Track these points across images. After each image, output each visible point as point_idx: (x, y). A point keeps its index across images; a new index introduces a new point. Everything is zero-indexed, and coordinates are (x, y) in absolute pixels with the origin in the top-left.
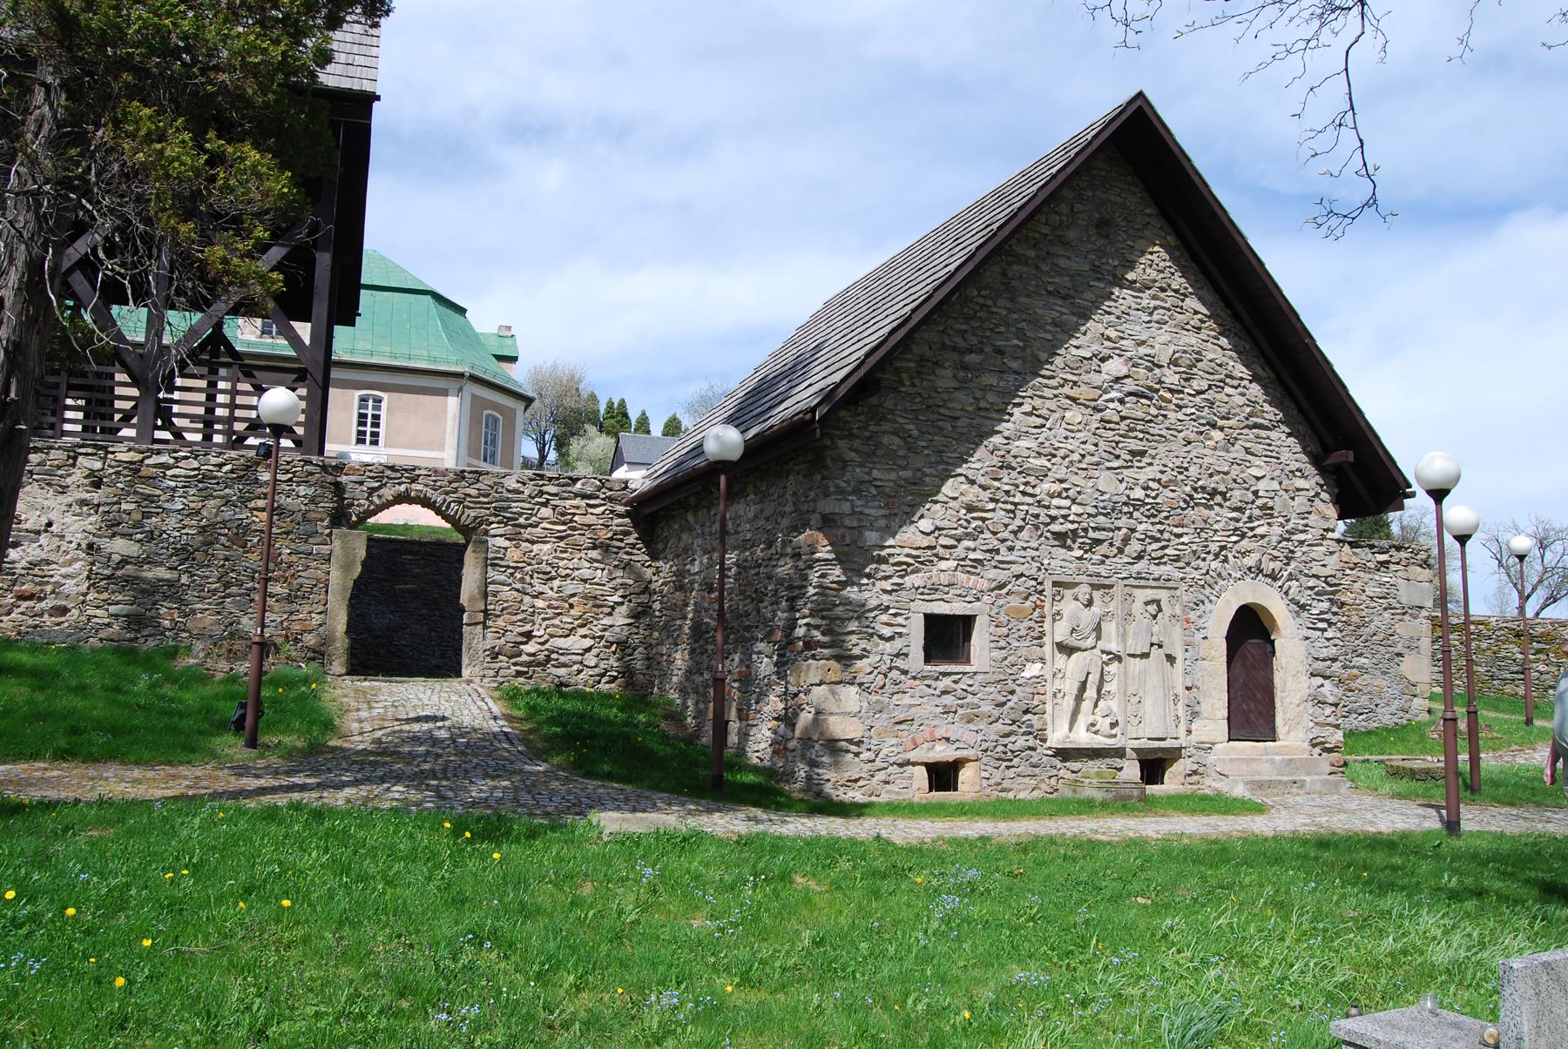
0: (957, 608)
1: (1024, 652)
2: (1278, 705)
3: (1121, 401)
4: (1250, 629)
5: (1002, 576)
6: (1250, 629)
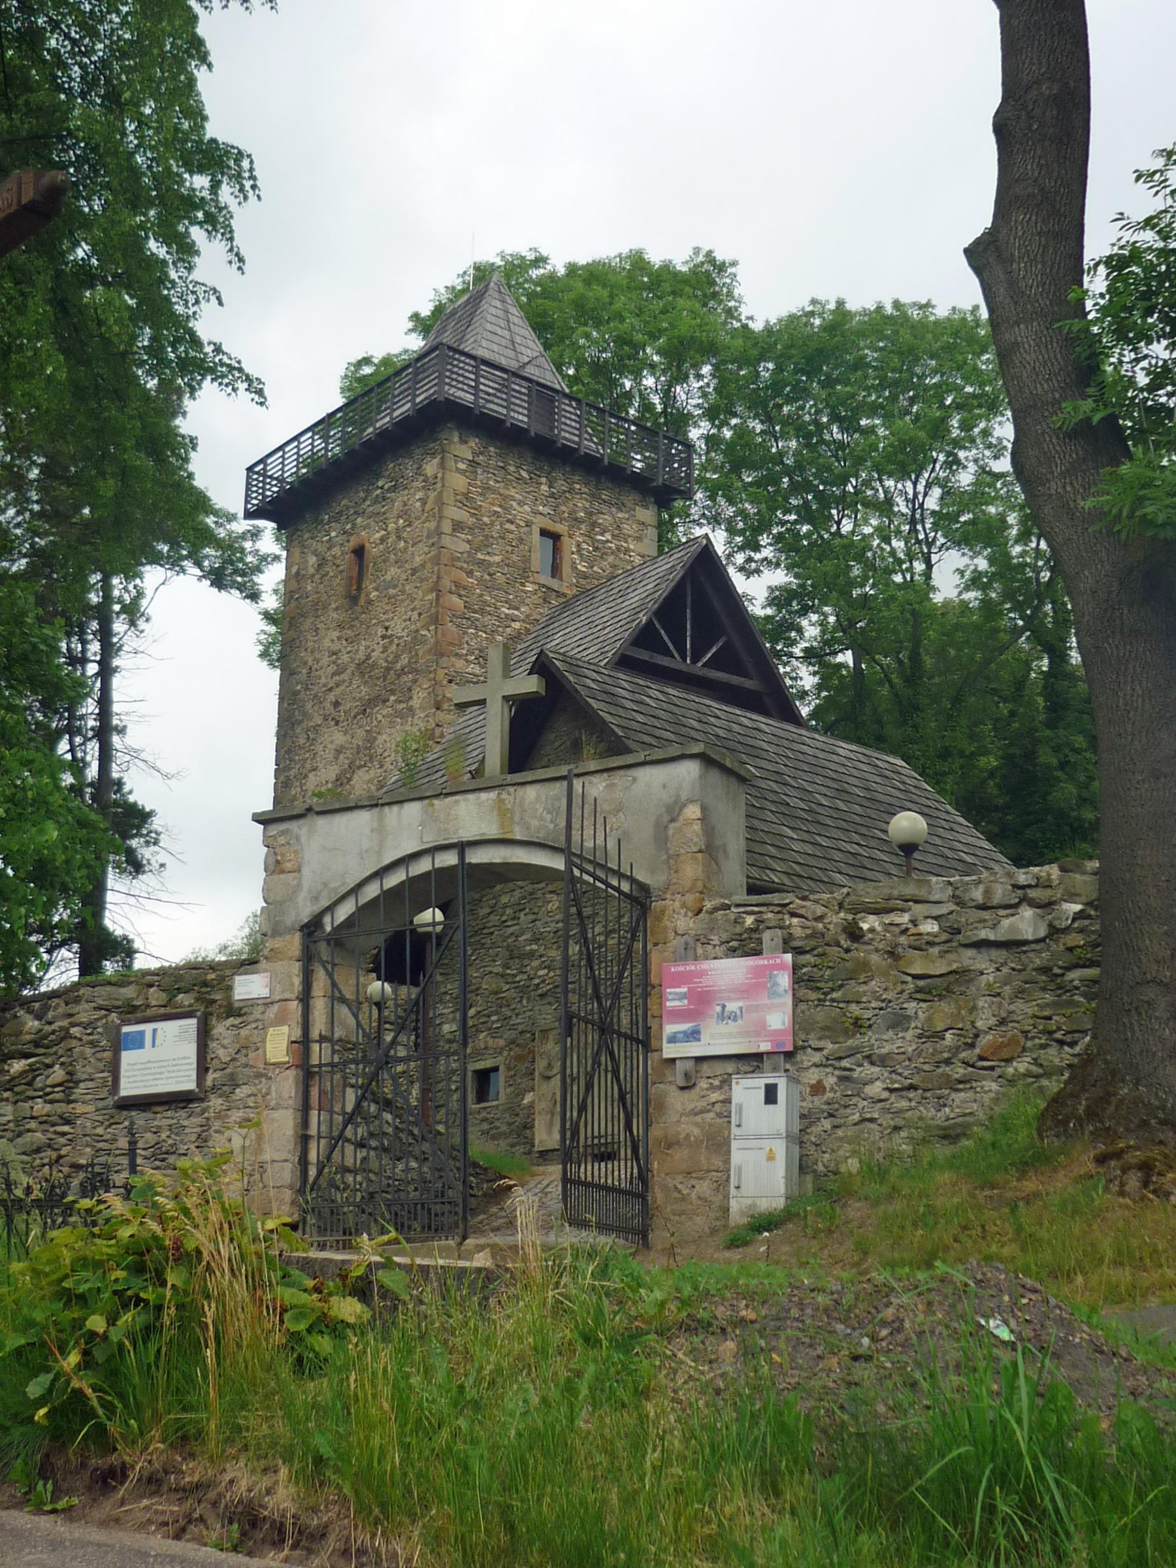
5: (512, 1034)
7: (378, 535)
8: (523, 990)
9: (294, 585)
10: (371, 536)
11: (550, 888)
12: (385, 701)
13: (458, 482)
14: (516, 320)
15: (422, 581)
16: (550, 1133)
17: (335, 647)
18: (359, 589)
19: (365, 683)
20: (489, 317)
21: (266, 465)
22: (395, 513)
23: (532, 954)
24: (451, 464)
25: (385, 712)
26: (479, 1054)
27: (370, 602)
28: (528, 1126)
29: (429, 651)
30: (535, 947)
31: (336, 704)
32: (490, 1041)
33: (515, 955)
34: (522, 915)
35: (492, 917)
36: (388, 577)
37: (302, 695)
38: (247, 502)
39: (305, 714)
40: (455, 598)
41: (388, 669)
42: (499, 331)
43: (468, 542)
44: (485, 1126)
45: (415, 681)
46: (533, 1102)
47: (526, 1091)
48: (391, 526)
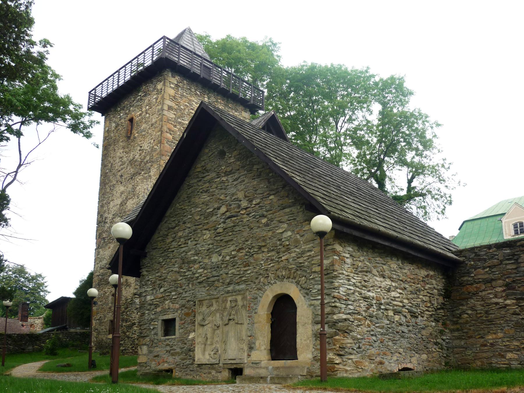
0: (170, 316)
1: (189, 329)
2: (169, 148)
3: (224, 222)
4: (283, 311)
5: (184, 302)
6: (283, 311)
7: (138, 113)
8: (189, 280)
9: (107, 134)
10: (136, 114)
11: (205, 227)
12: (140, 173)
13: (172, 92)
14: (196, 43)
15: (155, 128)
16: (204, 354)
17: (121, 155)
18: (131, 133)
19: (133, 168)
20: (185, 40)
21: (96, 90)
22: (145, 104)
23: (195, 261)
24: (167, 84)
25: (140, 178)
26: (164, 311)
27: (135, 138)
28: (191, 350)
29: (158, 154)
30: (196, 258)
31: (121, 176)
32: (171, 305)
33: (185, 261)
34: (189, 242)
35: (173, 243)
36: (142, 128)
37: (109, 174)
38: (89, 104)
39: (110, 181)
40: (168, 135)
41: (141, 162)
42: (189, 45)
43: (175, 114)
44: (168, 348)
45: (152, 166)
46: (194, 338)
47: (190, 332)
48: (144, 109)
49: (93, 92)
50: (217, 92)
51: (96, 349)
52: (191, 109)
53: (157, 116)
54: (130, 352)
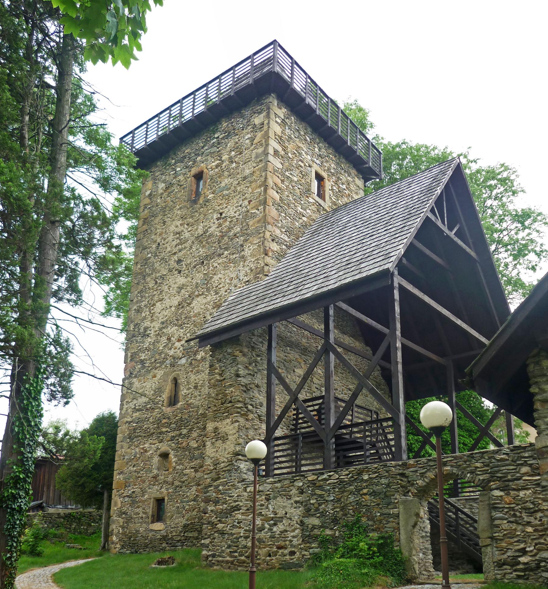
10: (209, 165)
13: (278, 129)
19: (204, 247)
22: (228, 149)
25: (220, 261)
29: (259, 222)
31: (179, 261)
39: (154, 270)
41: (222, 237)
48: (225, 157)
49: (128, 139)
50: (328, 143)
51: (123, 547)
52: (300, 160)
53: (255, 165)
54: (227, 562)
